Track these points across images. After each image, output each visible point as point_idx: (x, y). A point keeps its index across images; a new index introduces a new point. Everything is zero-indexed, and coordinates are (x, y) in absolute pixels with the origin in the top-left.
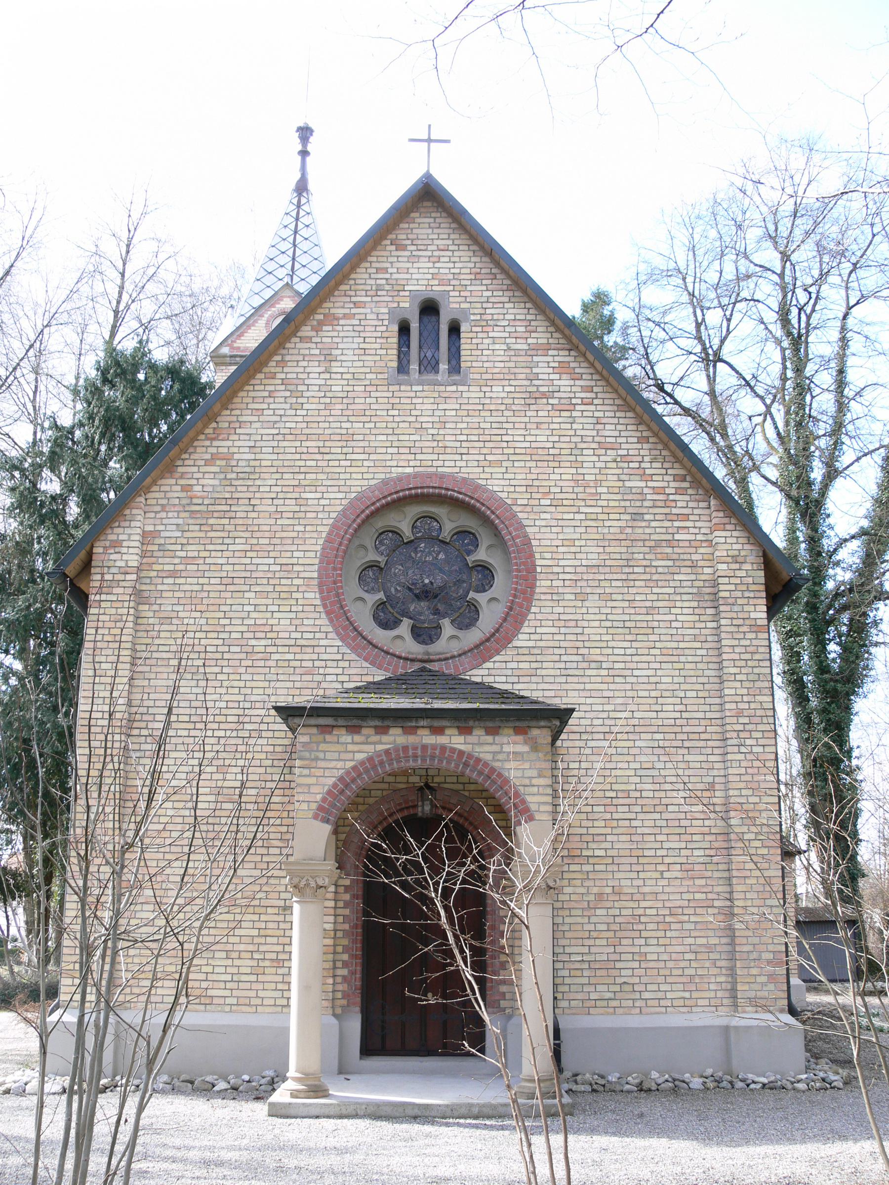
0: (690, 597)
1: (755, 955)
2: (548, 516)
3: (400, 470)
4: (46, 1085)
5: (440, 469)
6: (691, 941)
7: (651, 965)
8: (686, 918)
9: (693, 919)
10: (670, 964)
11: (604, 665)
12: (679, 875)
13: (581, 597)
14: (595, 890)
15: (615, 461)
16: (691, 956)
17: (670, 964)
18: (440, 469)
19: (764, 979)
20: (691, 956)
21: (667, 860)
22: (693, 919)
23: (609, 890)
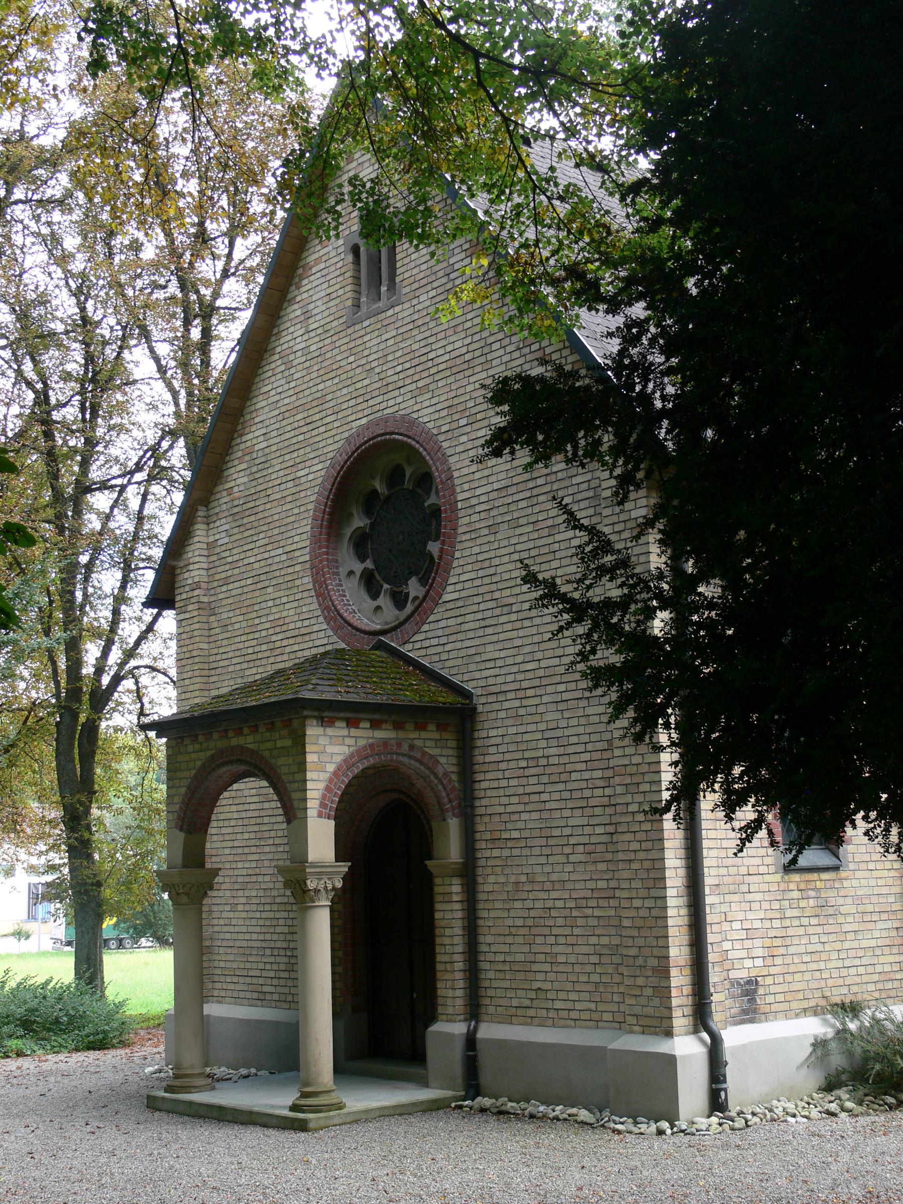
0: (222, 936)
1: (640, 961)
2: (464, 439)
3: (358, 423)
4: (147, 506)
5: (385, 412)
6: (594, 940)
7: (561, 968)
8: (589, 912)
9: (597, 913)
10: (577, 968)
11: (515, 608)
12: (582, 858)
13: (493, 529)
14: (513, 879)
15: (519, 349)
16: (594, 959)
17: (577, 968)
18: (385, 412)
19: (648, 992)
20: (594, 959)
21: (572, 841)
22: (597, 913)
23: (523, 879)
